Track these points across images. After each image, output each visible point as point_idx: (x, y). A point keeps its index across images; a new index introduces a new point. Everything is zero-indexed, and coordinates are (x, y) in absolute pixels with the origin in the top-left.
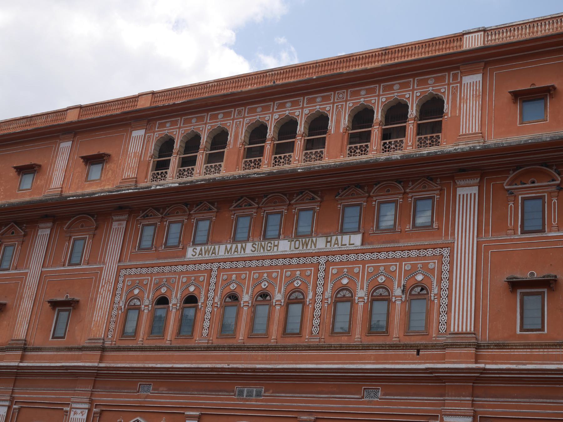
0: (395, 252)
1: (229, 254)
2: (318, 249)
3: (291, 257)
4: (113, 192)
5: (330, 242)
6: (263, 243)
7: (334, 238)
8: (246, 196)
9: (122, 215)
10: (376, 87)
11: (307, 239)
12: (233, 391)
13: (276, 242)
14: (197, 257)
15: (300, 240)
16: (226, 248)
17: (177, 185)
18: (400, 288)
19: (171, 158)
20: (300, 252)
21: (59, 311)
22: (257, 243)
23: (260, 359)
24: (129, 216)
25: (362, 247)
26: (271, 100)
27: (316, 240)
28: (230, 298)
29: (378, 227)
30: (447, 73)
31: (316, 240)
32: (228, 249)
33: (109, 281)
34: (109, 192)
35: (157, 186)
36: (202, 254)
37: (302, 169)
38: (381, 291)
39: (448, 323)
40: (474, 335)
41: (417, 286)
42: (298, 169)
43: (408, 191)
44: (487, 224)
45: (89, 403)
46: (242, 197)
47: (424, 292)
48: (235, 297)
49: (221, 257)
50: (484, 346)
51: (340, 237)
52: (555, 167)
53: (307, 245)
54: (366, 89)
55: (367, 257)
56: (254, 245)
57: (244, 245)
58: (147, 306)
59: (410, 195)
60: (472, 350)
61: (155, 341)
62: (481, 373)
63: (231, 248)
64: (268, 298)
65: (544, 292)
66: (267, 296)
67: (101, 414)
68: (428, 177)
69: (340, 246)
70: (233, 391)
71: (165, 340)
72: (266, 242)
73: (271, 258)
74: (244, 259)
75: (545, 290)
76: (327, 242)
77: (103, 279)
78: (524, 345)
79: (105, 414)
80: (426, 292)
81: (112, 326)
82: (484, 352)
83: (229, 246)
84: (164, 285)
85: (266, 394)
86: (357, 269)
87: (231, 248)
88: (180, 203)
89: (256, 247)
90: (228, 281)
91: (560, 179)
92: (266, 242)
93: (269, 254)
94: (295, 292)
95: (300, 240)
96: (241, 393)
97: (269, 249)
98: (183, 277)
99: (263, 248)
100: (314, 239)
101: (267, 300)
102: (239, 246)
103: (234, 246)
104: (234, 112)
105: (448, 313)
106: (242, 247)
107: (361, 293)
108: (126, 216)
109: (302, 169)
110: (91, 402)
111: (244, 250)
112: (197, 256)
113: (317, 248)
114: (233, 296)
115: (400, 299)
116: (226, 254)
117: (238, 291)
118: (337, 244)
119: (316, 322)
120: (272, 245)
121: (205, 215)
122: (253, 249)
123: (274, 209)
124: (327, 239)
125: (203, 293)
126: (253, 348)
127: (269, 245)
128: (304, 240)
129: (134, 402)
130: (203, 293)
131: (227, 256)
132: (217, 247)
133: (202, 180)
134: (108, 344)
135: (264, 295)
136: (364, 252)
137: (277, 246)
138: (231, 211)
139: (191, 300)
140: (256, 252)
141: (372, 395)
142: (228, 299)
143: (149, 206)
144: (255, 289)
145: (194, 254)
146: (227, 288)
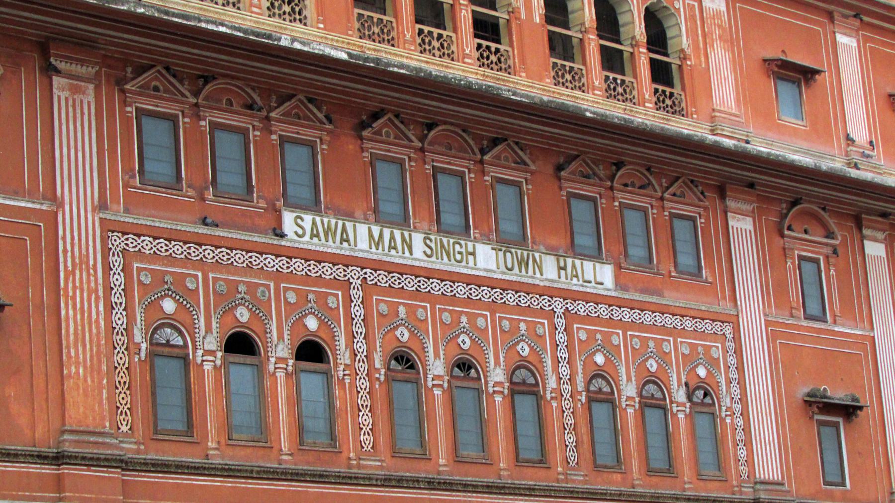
0: (320, 263)
1: (380, 250)
2: (547, 280)
3: (492, 283)
4: (174, 15)
5: (564, 268)
9: (82, 62)
14: (306, 242)
16: (371, 235)
17: (345, 56)
22: (432, 237)
27: (410, 236)
31: (410, 236)
32: (376, 235)
33: (84, 260)
34: (159, 10)
35: (294, 40)
37: (591, 113)
38: (599, 383)
39: (750, 462)
42: (586, 110)
47: (708, 400)
49: (361, 255)
55: (627, 315)
56: (428, 242)
58: (212, 353)
61: (536, 470)
63: (381, 235)
65: (838, 422)
66: (470, 368)
71: (275, 451)
73: (453, 278)
74: (403, 270)
75: (840, 420)
76: (560, 268)
77: (65, 251)
80: (710, 402)
81: (743, 453)
83: (376, 230)
84: (243, 302)
86: (581, 332)
89: (433, 245)
90: (391, 320)
91: (840, 238)
92: (452, 241)
93: (457, 270)
95: (513, 250)
97: (458, 257)
98: (286, 289)
101: (473, 379)
105: (748, 443)
107: (629, 390)
109: (594, 113)
112: (307, 238)
113: (544, 277)
115: (212, 358)
116: (374, 250)
117: (415, 346)
119: (570, 439)
121: (302, 130)
122: (429, 252)
123: (449, 163)
125: (342, 342)
126: (473, 486)
130: (342, 342)
131: (376, 254)
133: (402, 66)
136: (621, 304)
137: (473, 254)
139: (311, 352)
140: (434, 259)
143: (161, 62)
146: (390, 335)
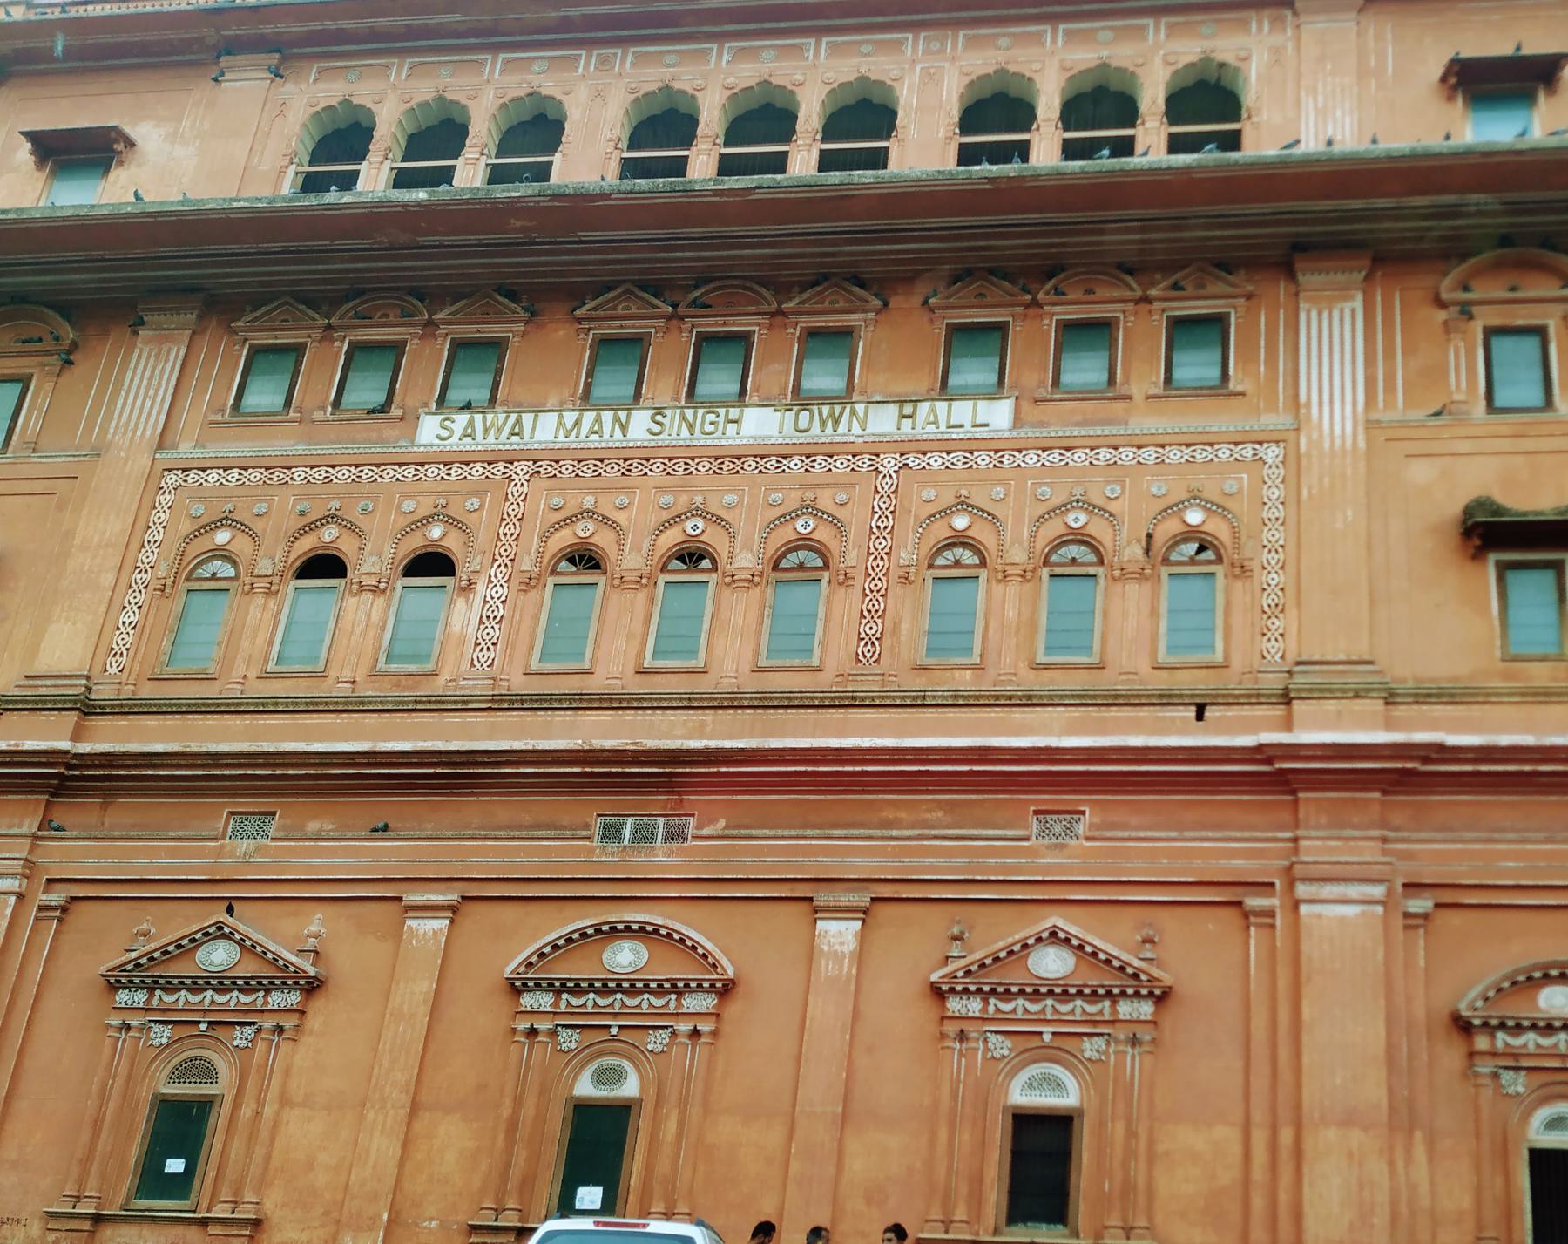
6: (689, 413)
7: (924, 407)
8: (633, 282)
10: (615, 55)
11: (837, 409)
12: (587, 826)
13: (734, 413)
15: (815, 409)
18: (1021, 544)
19: (363, 168)
20: (716, 442)
21: (1503, 568)
23: (679, 733)
24: (200, 317)
25: (1015, 434)
26: (580, 43)
28: (571, 560)
29: (1056, 382)
30: (910, 36)
31: (628, 416)
36: (472, 436)
40: (84, 682)
41: (1186, 540)
43: (1153, 292)
44: (1390, 387)
45: (24, 876)
46: (620, 283)
48: (591, 559)
50: (102, 707)
51: (945, 404)
52: (875, 288)
53: (836, 422)
54: (875, 42)
56: (659, 418)
57: (623, 415)
59: (1157, 305)
60: (1379, 705)
62: (1426, 760)
63: (577, 423)
64: (706, 563)
66: (701, 557)
67: (64, 910)
68: (413, 292)
69: (943, 428)
70: (587, 826)
72: (701, 411)
78: (1523, 694)
79: (84, 912)
82: (1400, 711)
83: (570, 418)
85: (705, 832)
87: (577, 423)
88: (398, 289)
89: (666, 421)
94: (796, 549)
96: (611, 833)
99: (691, 427)
100: (860, 408)
101: (703, 571)
102: (608, 416)
103: (589, 417)
104: (587, 62)
106: (617, 420)
108: (192, 317)
110: (30, 868)
111: (624, 428)
112: (454, 439)
113: (869, 431)
114: (581, 557)
118: (936, 422)
120: (721, 419)
122: (656, 428)
124: (901, 410)
127: (712, 417)
128: (826, 409)
129: (349, 868)
132: (527, 419)
134: (103, 693)
135: (691, 555)
138: (579, 321)
141: (1058, 829)
142: (564, 563)
144: (297, 544)
145: (445, 434)
